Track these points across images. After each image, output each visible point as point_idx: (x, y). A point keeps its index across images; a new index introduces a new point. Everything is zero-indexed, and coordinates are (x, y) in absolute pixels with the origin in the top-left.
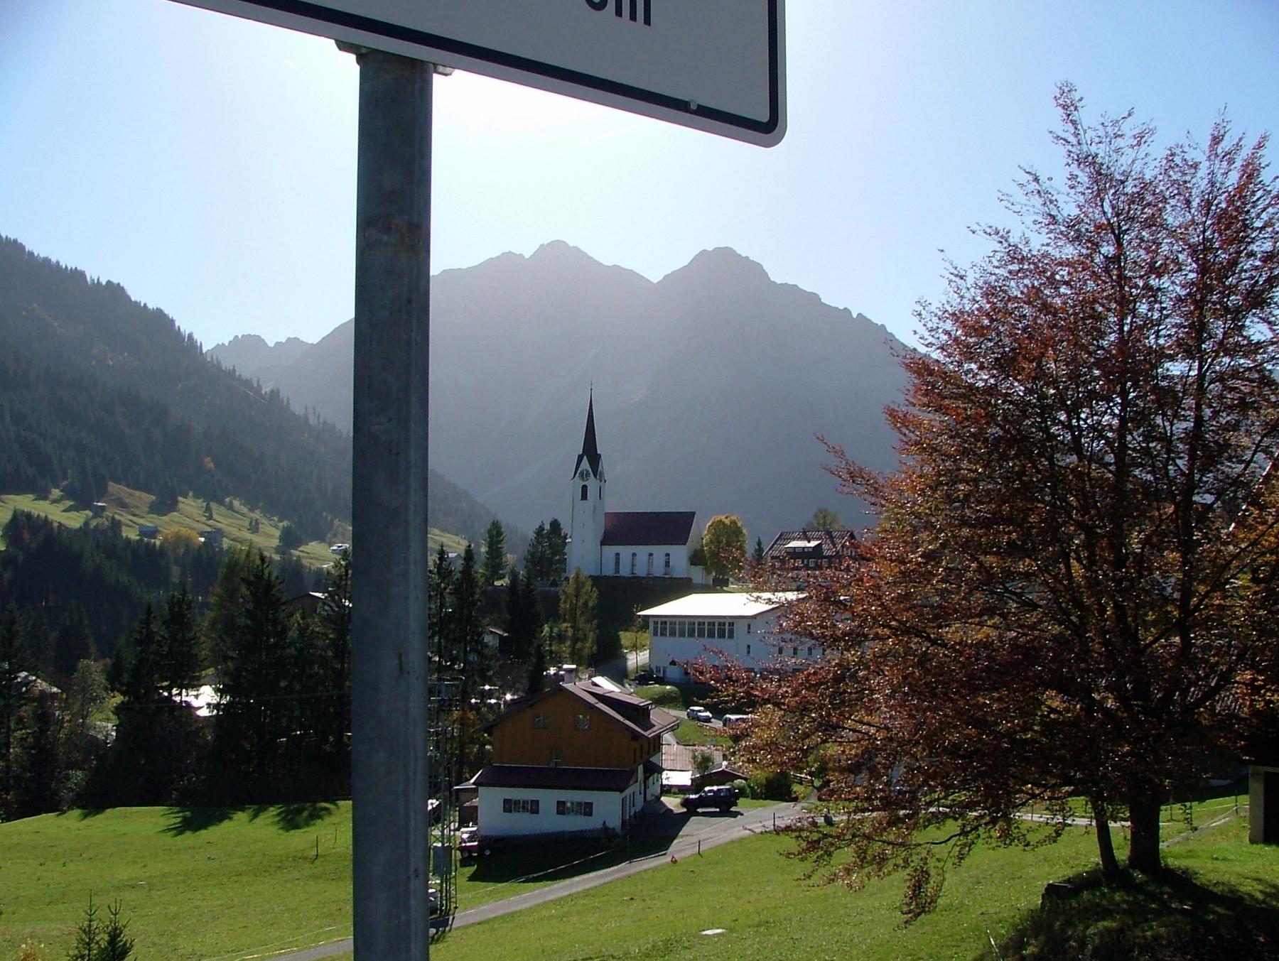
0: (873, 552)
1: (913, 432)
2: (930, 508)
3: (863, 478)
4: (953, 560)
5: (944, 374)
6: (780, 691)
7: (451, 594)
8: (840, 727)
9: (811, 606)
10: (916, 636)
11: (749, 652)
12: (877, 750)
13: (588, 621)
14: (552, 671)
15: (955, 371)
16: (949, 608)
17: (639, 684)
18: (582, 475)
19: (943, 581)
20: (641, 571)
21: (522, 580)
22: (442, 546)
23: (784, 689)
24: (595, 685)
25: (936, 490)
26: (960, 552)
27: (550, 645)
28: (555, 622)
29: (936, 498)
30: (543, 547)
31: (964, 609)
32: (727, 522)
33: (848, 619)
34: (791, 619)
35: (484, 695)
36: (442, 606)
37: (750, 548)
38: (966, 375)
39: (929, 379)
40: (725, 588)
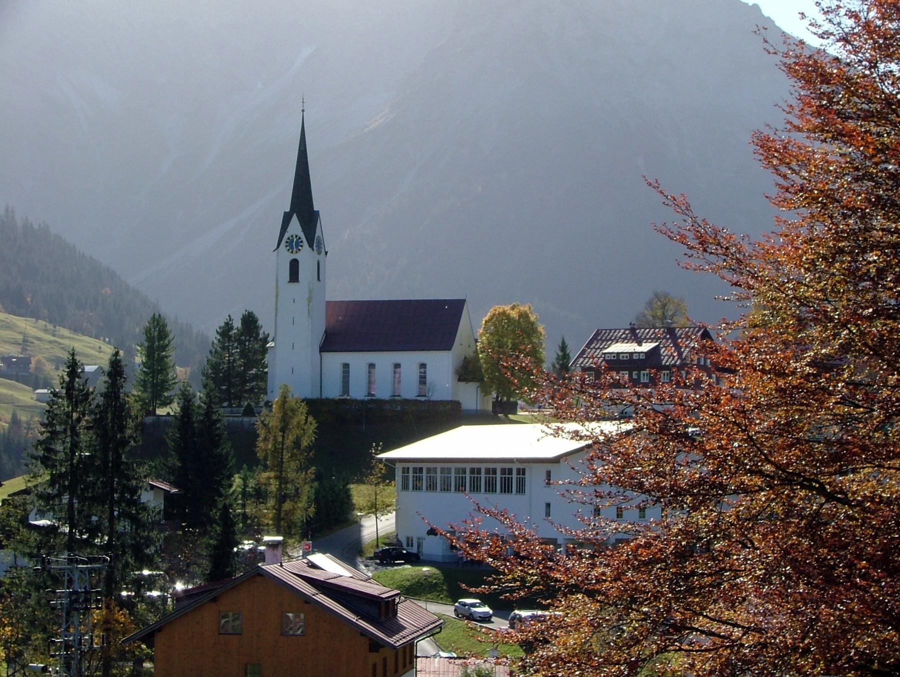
0: (735, 359)
1: (797, 174)
2: (822, 290)
3: (719, 244)
4: (858, 370)
5: (848, 83)
6: (594, 573)
7: (88, 428)
8: (688, 628)
9: (640, 442)
10: (803, 487)
11: (548, 514)
12: (745, 662)
13: (300, 469)
14: (247, 545)
15: (865, 76)
16: (853, 444)
17: (382, 564)
18: (290, 243)
19: (843, 401)
20: (383, 392)
21: (199, 407)
22: (73, 355)
23: (600, 570)
24: (313, 566)
25: (832, 263)
26: (871, 357)
27: (244, 506)
28: (250, 469)
29: (833, 274)
30: (231, 355)
31: (877, 446)
32: (514, 314)
33: (696, 462)
34: (610, 462)
35: (140, 584)
36: (75, 446)
37: (549, 355)
38: (882, 81)
39: (825, 88)
40: (511, 416)
